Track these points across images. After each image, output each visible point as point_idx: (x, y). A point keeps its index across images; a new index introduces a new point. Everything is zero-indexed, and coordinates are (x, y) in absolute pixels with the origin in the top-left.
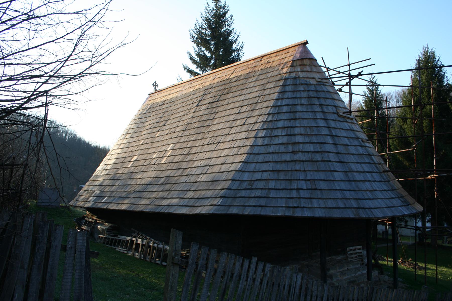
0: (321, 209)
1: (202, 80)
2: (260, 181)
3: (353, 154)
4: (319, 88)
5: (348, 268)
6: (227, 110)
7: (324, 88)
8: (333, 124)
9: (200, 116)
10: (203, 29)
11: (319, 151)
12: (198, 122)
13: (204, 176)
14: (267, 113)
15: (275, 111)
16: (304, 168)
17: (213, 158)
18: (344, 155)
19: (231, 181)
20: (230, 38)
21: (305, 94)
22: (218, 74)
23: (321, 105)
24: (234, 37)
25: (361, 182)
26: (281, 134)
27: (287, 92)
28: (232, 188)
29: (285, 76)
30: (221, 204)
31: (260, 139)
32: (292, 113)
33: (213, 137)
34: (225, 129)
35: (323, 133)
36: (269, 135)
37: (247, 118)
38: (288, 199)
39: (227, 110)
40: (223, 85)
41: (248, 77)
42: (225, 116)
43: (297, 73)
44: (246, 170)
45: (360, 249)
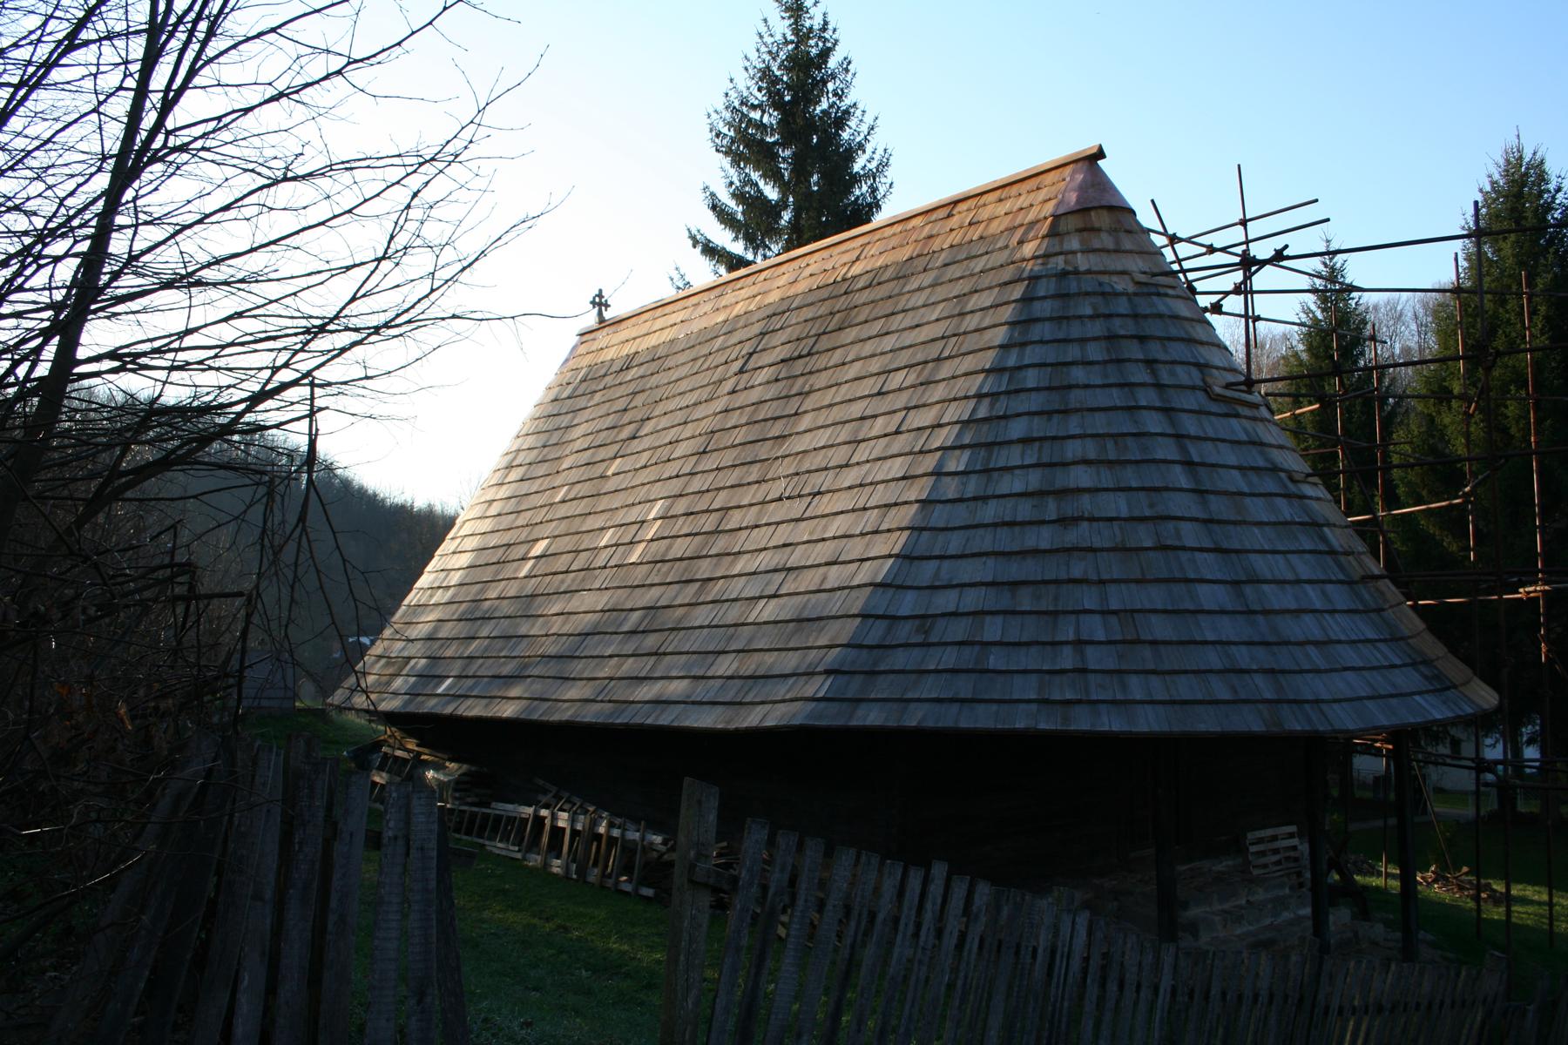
2: (953, 618)
3: (1260, 524)
4: (1144, 307)
6: (840, 384)
7: (1161, 306)
8: (1190, 425)
9: (753, 404)
10: (754, 107)
11: (1147, 514)
15: (999, 386)
17: (798, 544)
18: (1231, 527)
19: (859, 619)
20: (845, 135)
21: (1097, 328)
22: (808, 265)
26: (1019, 463)
29: (1031, 270)
30: (827, 696)
33: (797, 474)
34: (834, 449)
35: (1160, 455)
37: (908, 409)
38: (1047, 677)
39: (840, 384)
40: (825, 300)
41: (909, 272)
43: (1070, 257)
44: (909, 583)
45: (1291, 835)
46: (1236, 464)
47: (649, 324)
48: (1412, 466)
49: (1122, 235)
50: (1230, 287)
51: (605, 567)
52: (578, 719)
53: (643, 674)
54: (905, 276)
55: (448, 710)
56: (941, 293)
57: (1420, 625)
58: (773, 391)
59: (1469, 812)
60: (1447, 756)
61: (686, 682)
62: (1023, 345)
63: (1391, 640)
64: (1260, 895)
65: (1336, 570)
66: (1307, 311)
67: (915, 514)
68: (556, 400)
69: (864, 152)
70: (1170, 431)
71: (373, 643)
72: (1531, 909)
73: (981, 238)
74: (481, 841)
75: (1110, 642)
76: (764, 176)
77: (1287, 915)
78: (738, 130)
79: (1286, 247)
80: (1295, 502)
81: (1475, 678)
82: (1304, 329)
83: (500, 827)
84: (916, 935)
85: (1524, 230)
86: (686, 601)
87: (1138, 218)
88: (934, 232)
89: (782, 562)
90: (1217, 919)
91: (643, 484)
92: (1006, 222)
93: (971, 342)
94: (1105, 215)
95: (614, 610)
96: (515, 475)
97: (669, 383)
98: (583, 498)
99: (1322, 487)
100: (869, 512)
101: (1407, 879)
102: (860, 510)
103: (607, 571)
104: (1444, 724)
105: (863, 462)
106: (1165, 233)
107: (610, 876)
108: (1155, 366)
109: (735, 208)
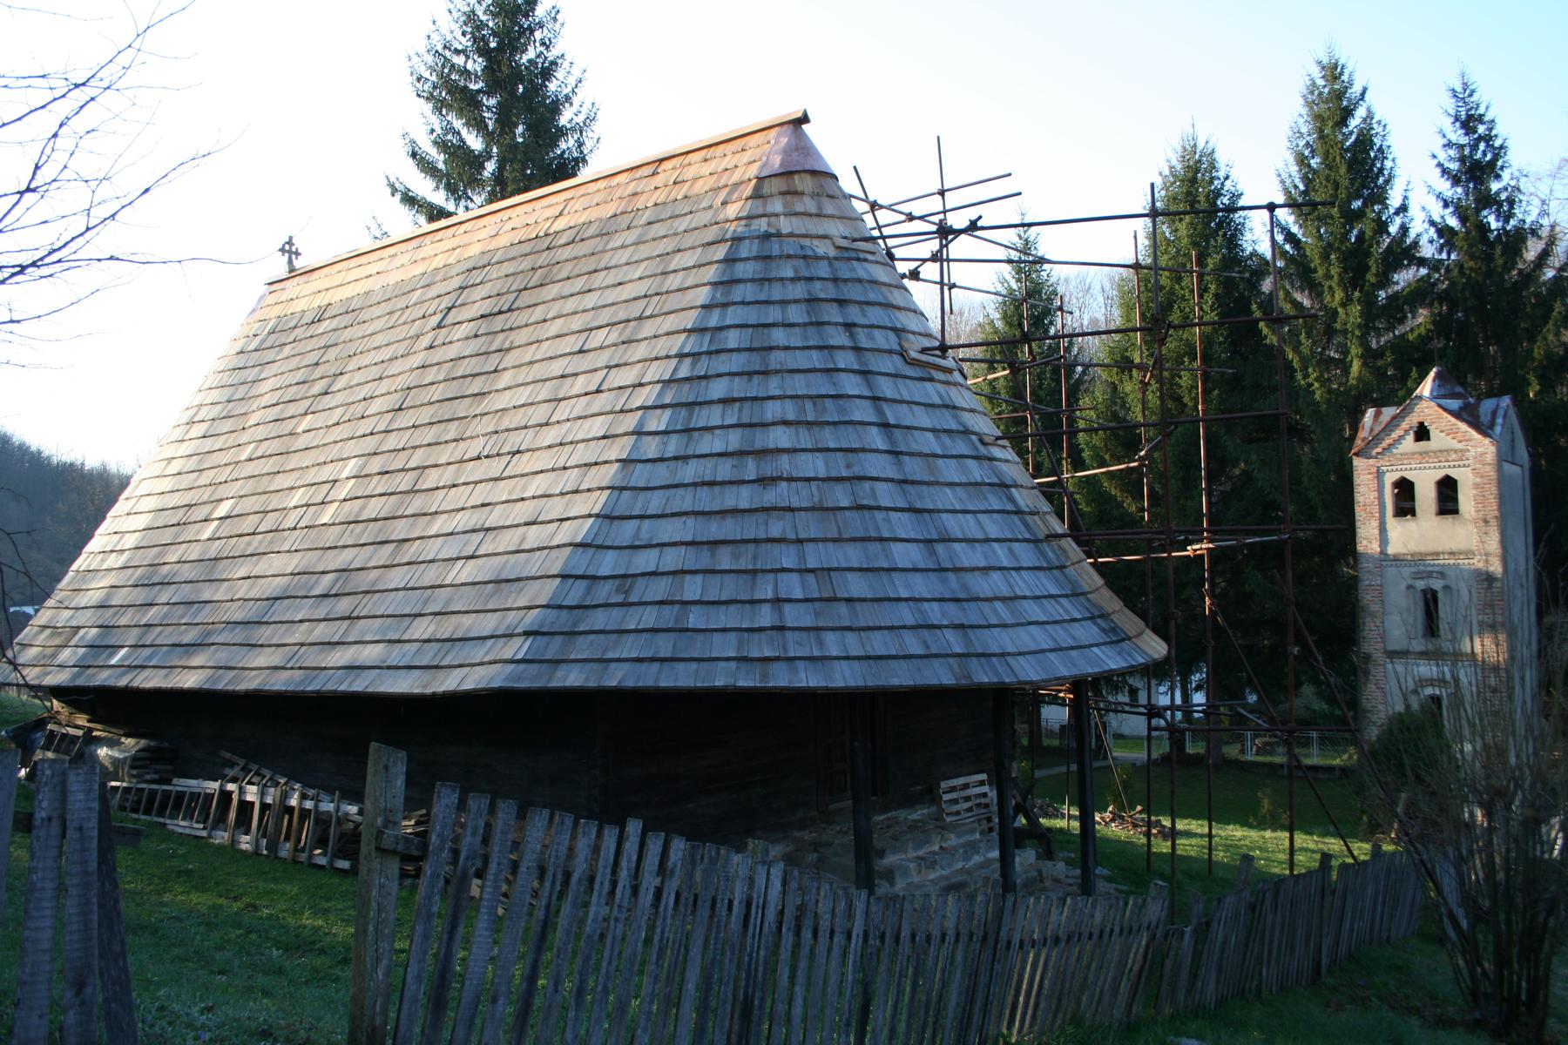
3: (951, 484)
4: (844, 271)
5: (944, 845)
7: (861, 271)
8: (886, 388)
10: (457, 52)
17: (497, 504)
18: (924, 488)
19: (559, 580)
20: (552, 86)
21: (798, 291)
25: (977, 573)
26: (720, 423)
27: (739, 281)
33: (496, 432)
35: (857, 417)
37: (609, 367)
38: (746, 635)
40: (526, 255)
41: (613, 229)
43: (773, 219)
44: (609, 543)
45: (982, 783)
46: (930, 426)
47: (343, 274)
48: (1096, 430)
49: (825, 200)
50: (928, 255)
51: (295, 529)
52: (267, 688)
53: (335, 639)
55: (123, 682)
56: (644, 250)
57: (1099, 581)
59: (1141, 755)
60: (1127, 704)
61: (381, 646)
62: (725, 305)
63: (1072, 595)
64: (953, 841)
65: (1023, 529)
66: (1003, 281)
67: (616, 474)
68: (242, 352)
69: (571, 104)
70: (867, 393)
71: (37, 611)
72: (1194, 841)
73: (686, 197)
74: (161, 820)
75: (807, 600)
76: (467, 124)
77: (977, 859)
78: (441, 76)
79: (980, 217)
80: (986, 463)
81: (1148, 632)
82: (1000, 299)
83: (180, 804)
84: (612, 892)
85: (1197, 212)
86: (381, 563)
87: (840, 183)
88: (639, 190)
89: (480, 522)
90: (912, 865)
91: (336, 442)
93: (674, 301)
94: (808, 178)
95: (304, 573)
96: (198, 430)
97: (364, 337)
98: (270, 456)
99: (1010, 450)
100: (569, 471)
101: (1086, 820)
102: (559, 469)
103: (297, 532)
104: (1123, 673)
105: (564, 421)
106: (866, 200)
107: (303, 850)
108: (854, 329)
109: (437, 156)
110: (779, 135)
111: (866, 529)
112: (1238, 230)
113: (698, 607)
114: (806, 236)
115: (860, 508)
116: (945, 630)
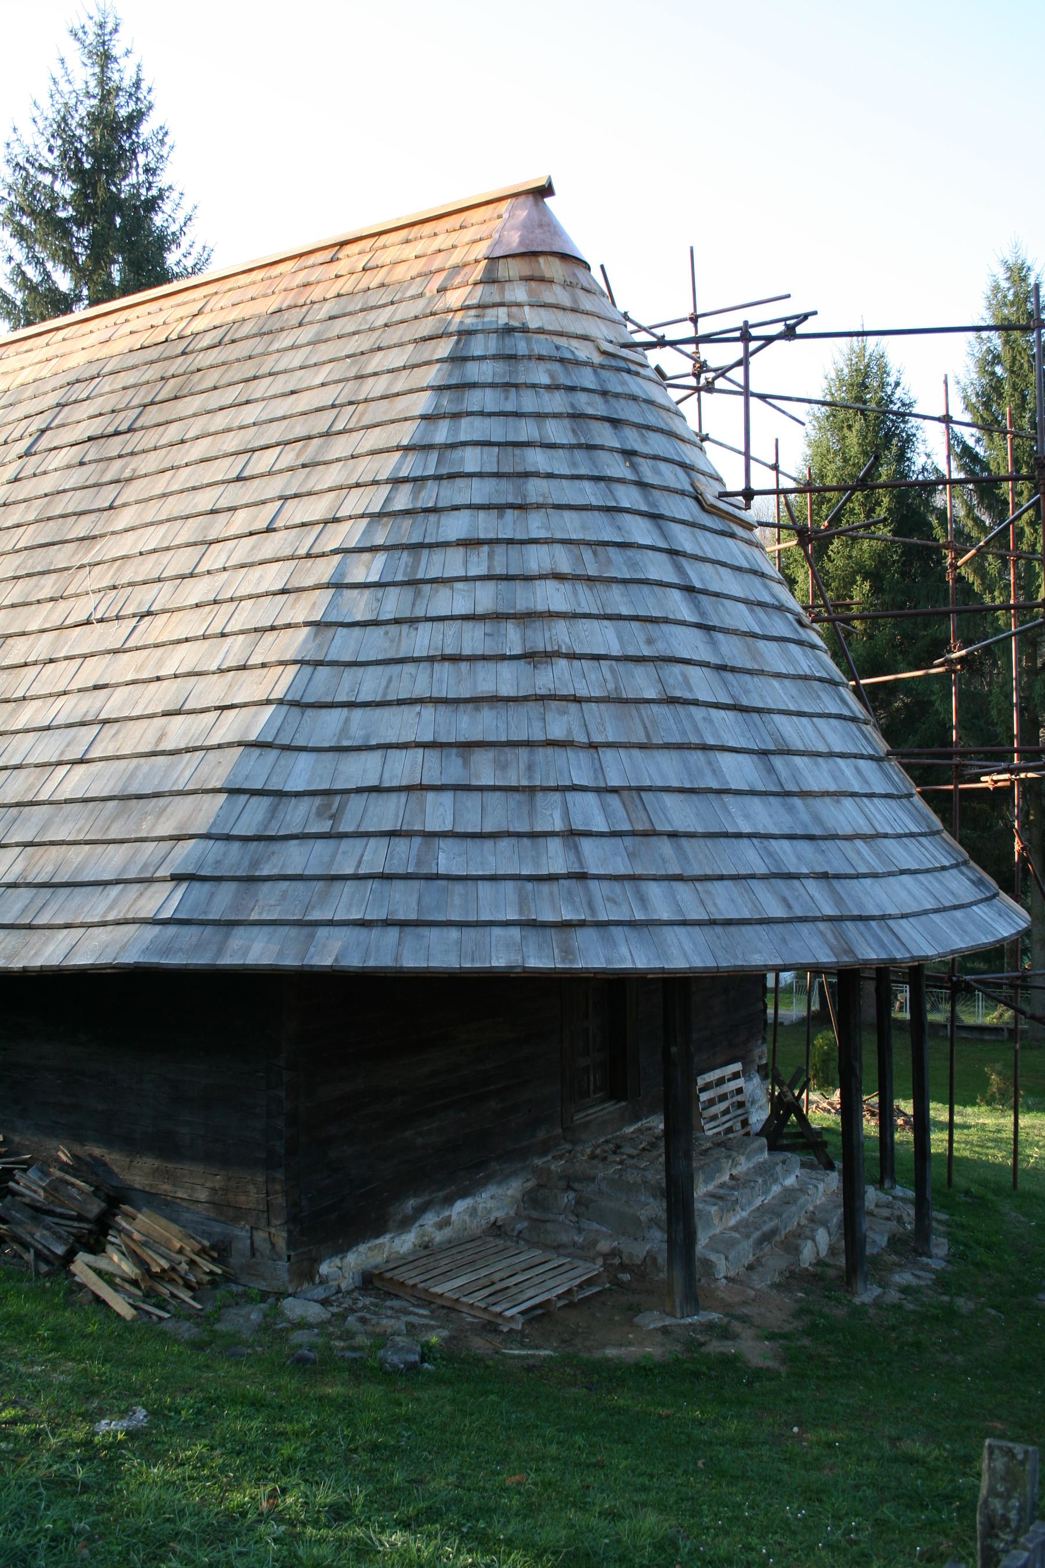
0: (689, 928)
1: (47, 345)
2: (374, 795)
3: (778, 675)
4: (614, 383)
5: (734, 1172)
6: (178, 468)
7: (634, 385)
8: (684, 539)
9: (46, 495)
10: (42, 169)
11: (646, 654)
12: (37, 521)
13: (72, 773)
14: (383, 476)
15: (425, 468)
16: (588, 735)
17: (118, 685)
18: (747, 677)
19: (224, 796)
20: (158, 220)
21: (557, 402)
22: (127, 321)
23: (629, 454)
24: (170, 220)
25: (827, 800)
26: (461, 573)
27: (474, 385)
28: (235, 832)
29: (461, 322)
30: (177, 916)
31: (362, 595)
32: (504, 481)
33: (115, 587)
34: (173, 552)
35: (653, 575)
36: (404, 574)
37: (286, 498)
38: (529, 886)
39: (178, 468)
40: (152, 362)
41: (278, 326)
42: (171, 494)
43: (514, 309)
44: (300, 742)
45: (736, 1076)
54: (271, 332)
56: (325, 351)
58: (77, 477)
62: (456, 416)
67: (305, 641)
75: (614, 834)
92: (418, 266)
100: (230, 639)
105: (218, 570)
110: (513, 208)
111: (684, 733)
112: (908, 441)
113: (450, 841)
114: (561, 334)
115: (672, 701)
116: (804, 881)
